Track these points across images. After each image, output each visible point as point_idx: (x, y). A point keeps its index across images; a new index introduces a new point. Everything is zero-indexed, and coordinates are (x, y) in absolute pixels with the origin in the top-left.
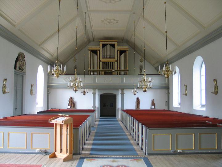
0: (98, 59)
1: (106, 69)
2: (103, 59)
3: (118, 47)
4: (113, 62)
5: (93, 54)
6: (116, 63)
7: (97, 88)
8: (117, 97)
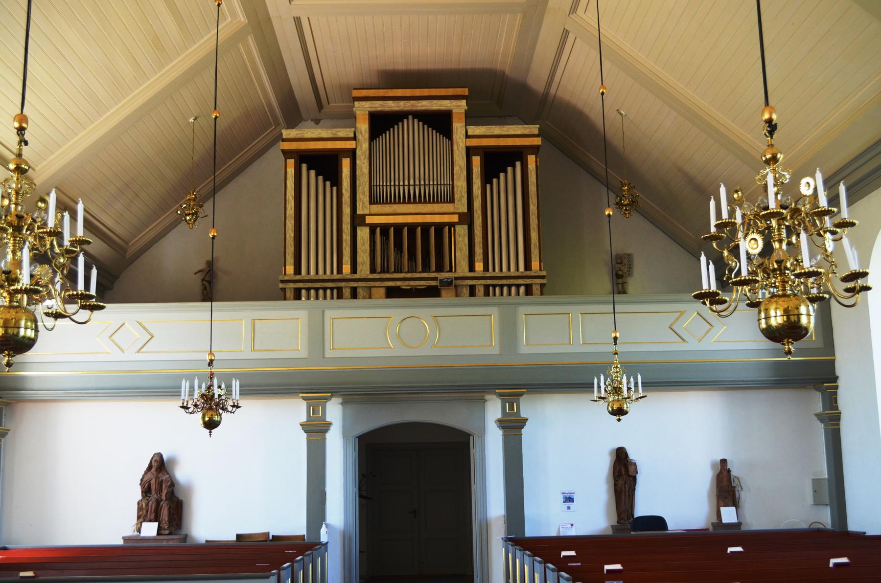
0: (347, 210)
1: (398, 270)
2: (376, 208)
3: (473, 130)
4: (439, 227)
5: (310, 177)
6: (462, 231)
7: (334, 393)
8: (474, 452)
